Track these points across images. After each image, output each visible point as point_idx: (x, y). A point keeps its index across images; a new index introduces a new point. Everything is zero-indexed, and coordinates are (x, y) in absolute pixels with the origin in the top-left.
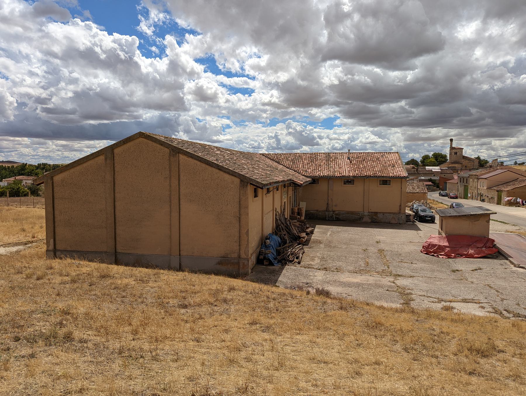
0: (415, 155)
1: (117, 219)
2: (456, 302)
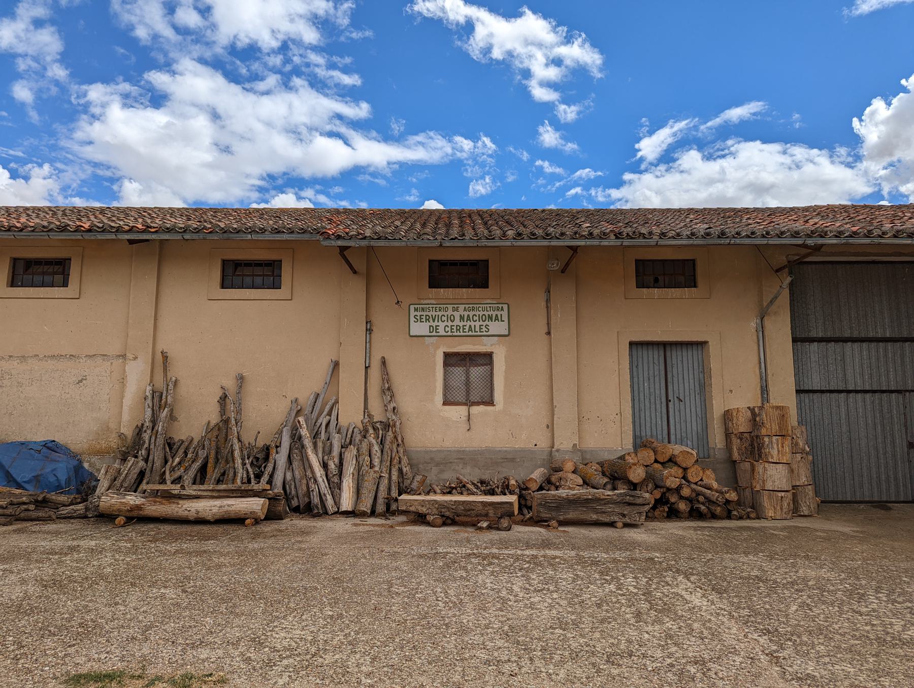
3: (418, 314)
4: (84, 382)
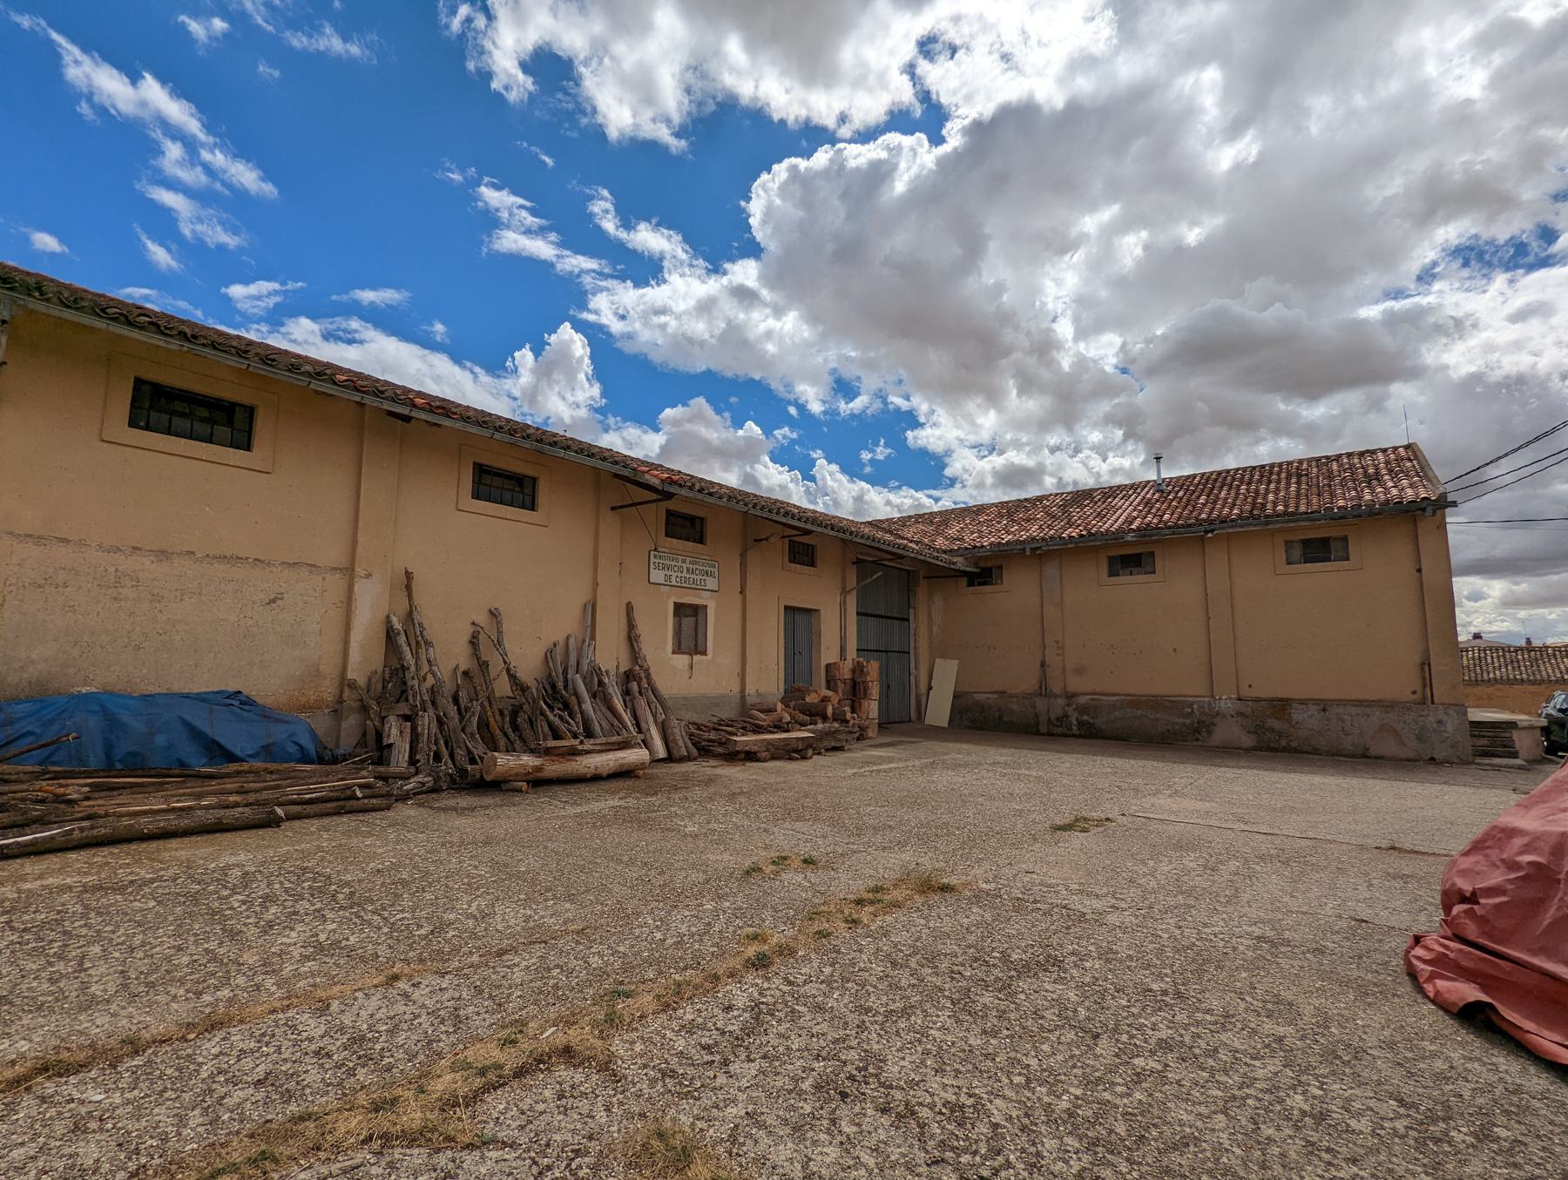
3: (657, 561)
4: (279, 602)
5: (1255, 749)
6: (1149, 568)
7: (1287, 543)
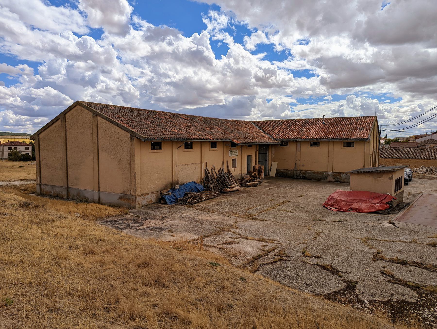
0: (66, 97)
1: (68, 164)
2: (253, 240)
5: (335, 181)
6: (318, 145)
7: (344, 142)
